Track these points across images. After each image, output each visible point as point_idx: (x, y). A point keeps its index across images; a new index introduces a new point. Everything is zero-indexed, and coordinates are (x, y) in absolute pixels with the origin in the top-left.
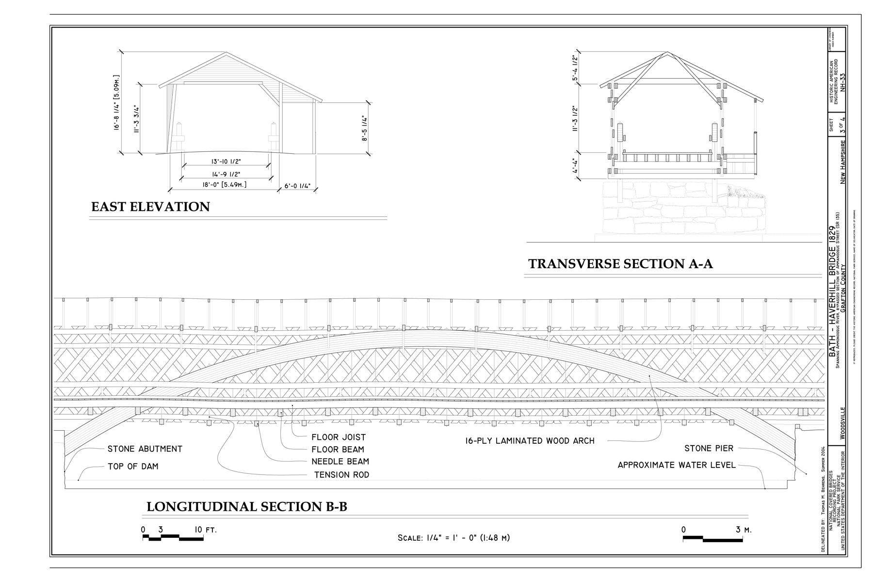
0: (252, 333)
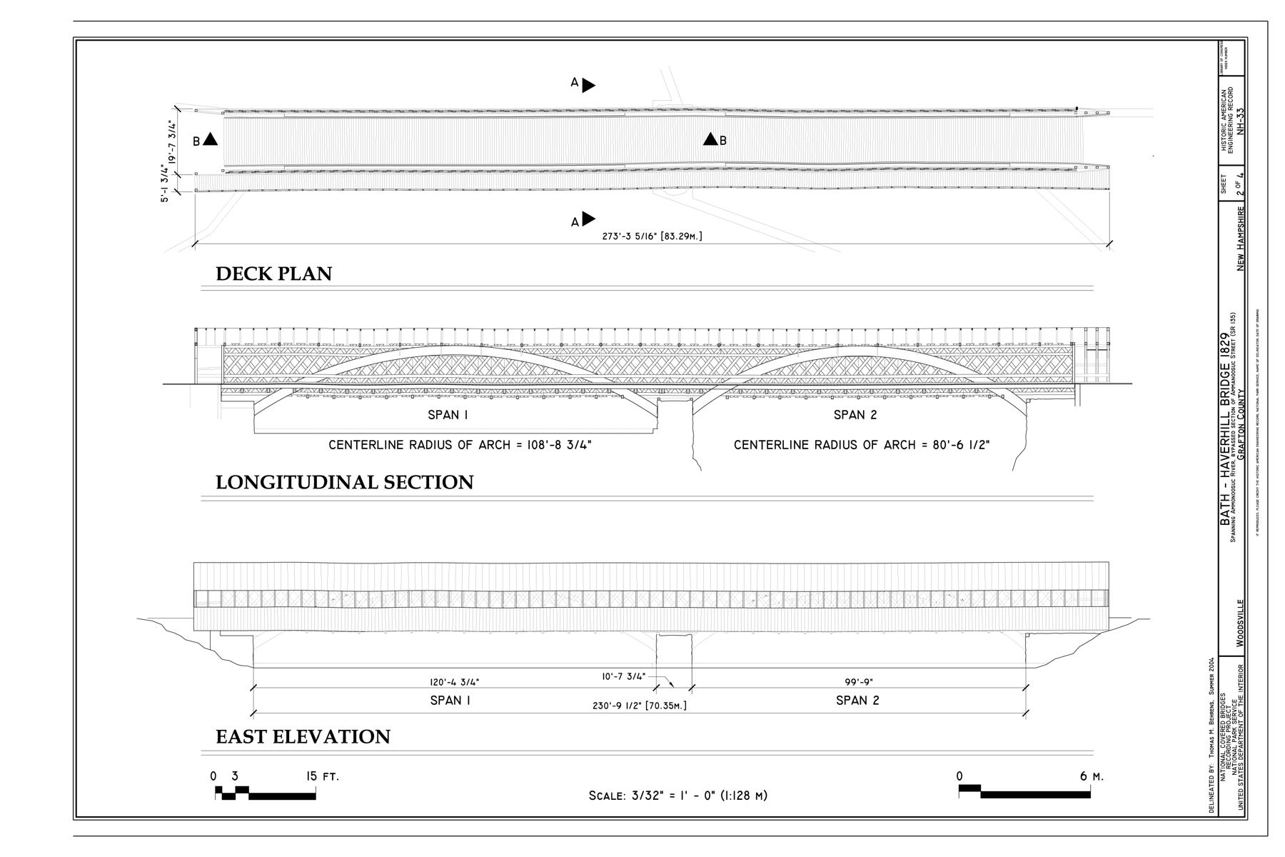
0: (358, 347)
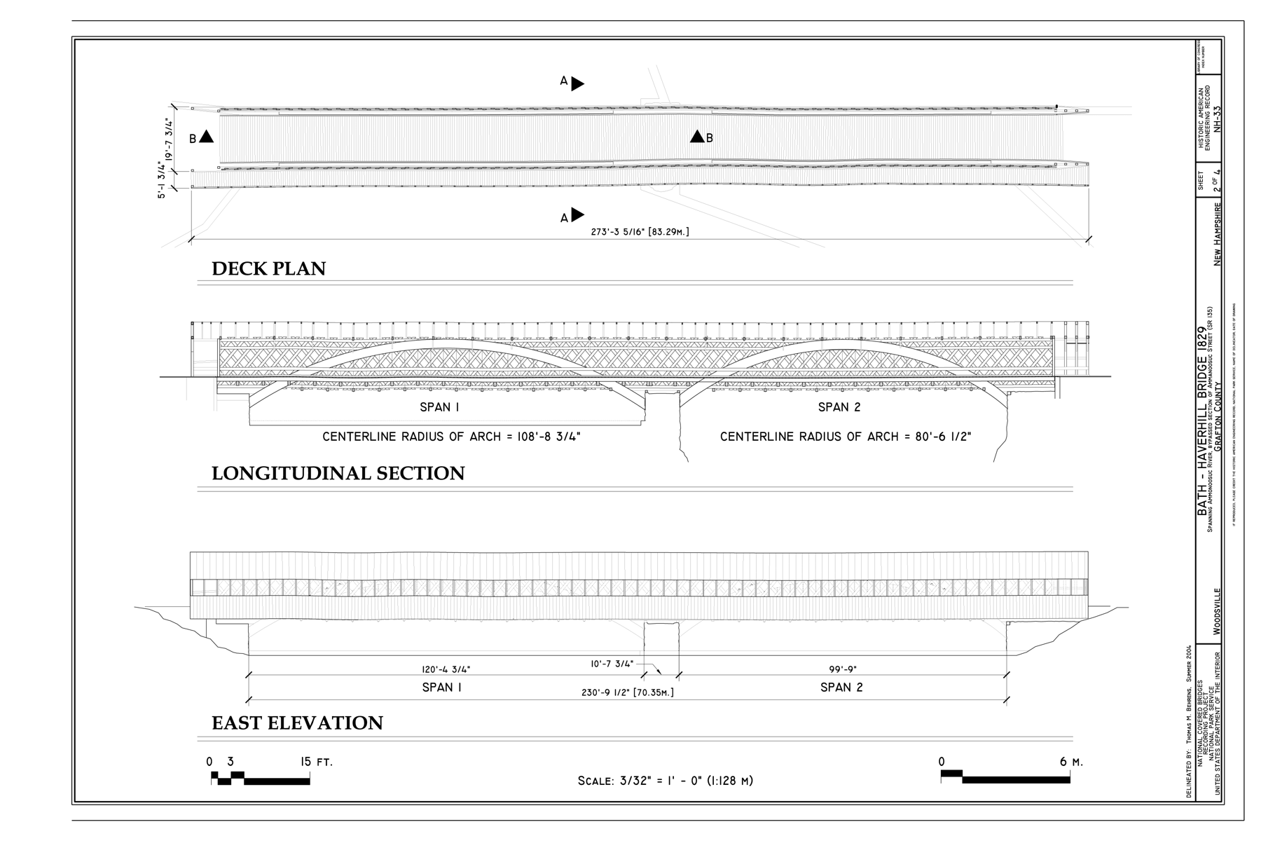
0: (351, 341)
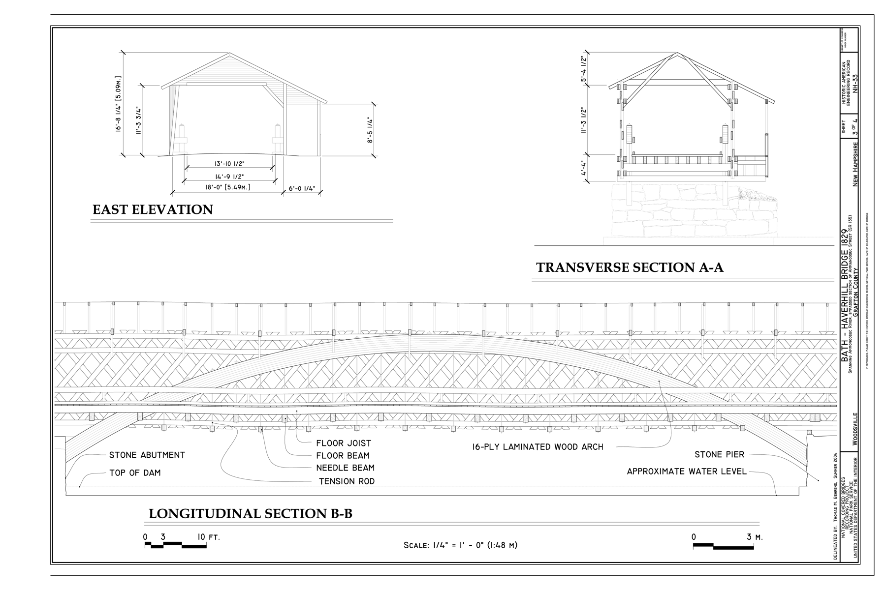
0: (256, 338)
